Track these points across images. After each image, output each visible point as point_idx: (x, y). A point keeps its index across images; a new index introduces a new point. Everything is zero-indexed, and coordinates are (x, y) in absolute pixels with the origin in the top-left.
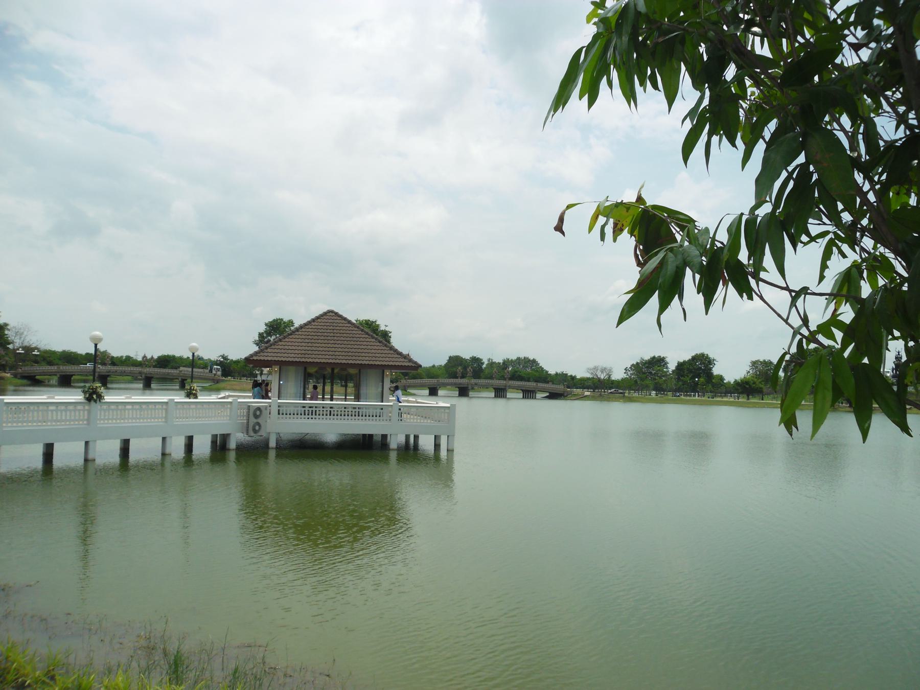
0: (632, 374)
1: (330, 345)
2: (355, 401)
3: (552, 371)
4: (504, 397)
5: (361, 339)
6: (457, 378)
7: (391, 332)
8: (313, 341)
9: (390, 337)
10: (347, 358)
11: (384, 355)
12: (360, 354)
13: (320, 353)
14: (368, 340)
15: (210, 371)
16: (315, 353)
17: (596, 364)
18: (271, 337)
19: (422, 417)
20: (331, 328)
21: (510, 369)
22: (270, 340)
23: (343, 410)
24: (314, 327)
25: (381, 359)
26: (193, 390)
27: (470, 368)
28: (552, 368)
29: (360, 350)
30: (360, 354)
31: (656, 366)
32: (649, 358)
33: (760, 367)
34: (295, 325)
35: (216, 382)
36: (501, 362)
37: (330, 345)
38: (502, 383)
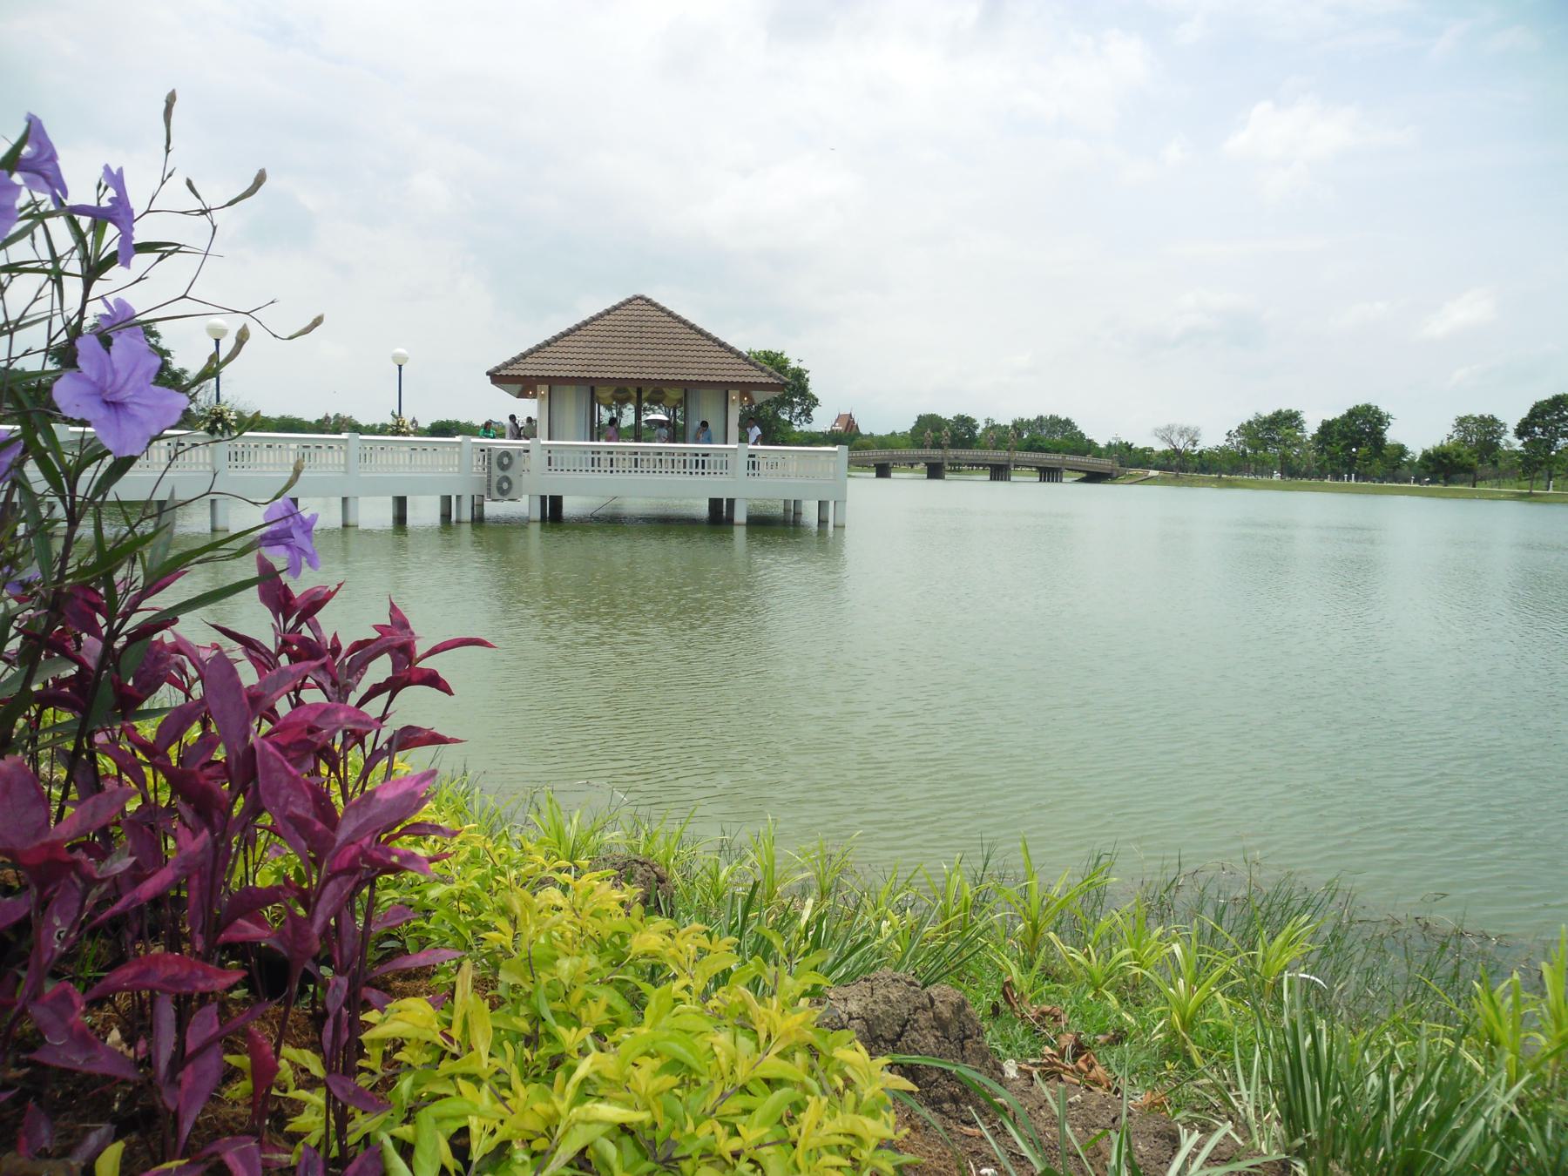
0: (1238, 442)
7: (808, 372)
9: (808, 380)
10: (661, 370)
14: (699, 342)
17: (1172, 422)
20: (638, 323)
21: (1025, 436)
26: (403, 426)
29: (684, 359)
31: (1284, 428)
33: (1473, 427)
37: (633, 351)
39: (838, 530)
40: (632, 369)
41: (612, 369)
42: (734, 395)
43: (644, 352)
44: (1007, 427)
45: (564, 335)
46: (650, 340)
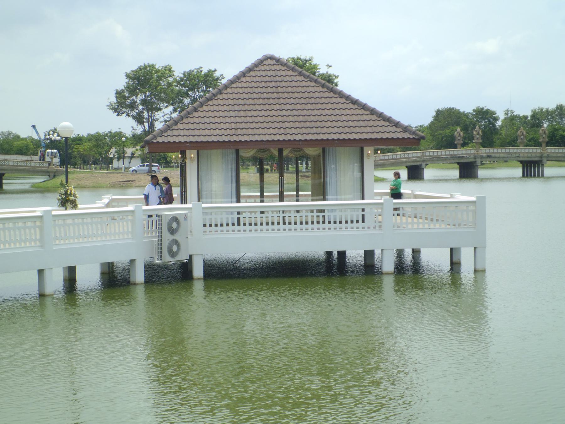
1: (273, 113)
2: (312, 200)
4: (539, 176)
5: (323, 100)
6: (455, 147)
7: (337, 77)
8: (246, 107)
10: (304, 130)
11: (362, 123)
12: (324, 124)
13: (259, 125)
14: (334, 100)
15: (40, 157)
16: (252, 126)
18: (137, 96)
19: (426, 219)
20: (273, 84)
22: (136, 102)
23: (258, 215)
24: (245, 85)
26: (70, 194)
27: (477, 128)
29: (323, 118)
34: (174, 73)
35: (52, 175)
38: (533, 152)
39: (479, 274)
40: (276, 131)
41: (258, 132)
43: (284, 113)
44: (526, 117)
46: (287, 101)
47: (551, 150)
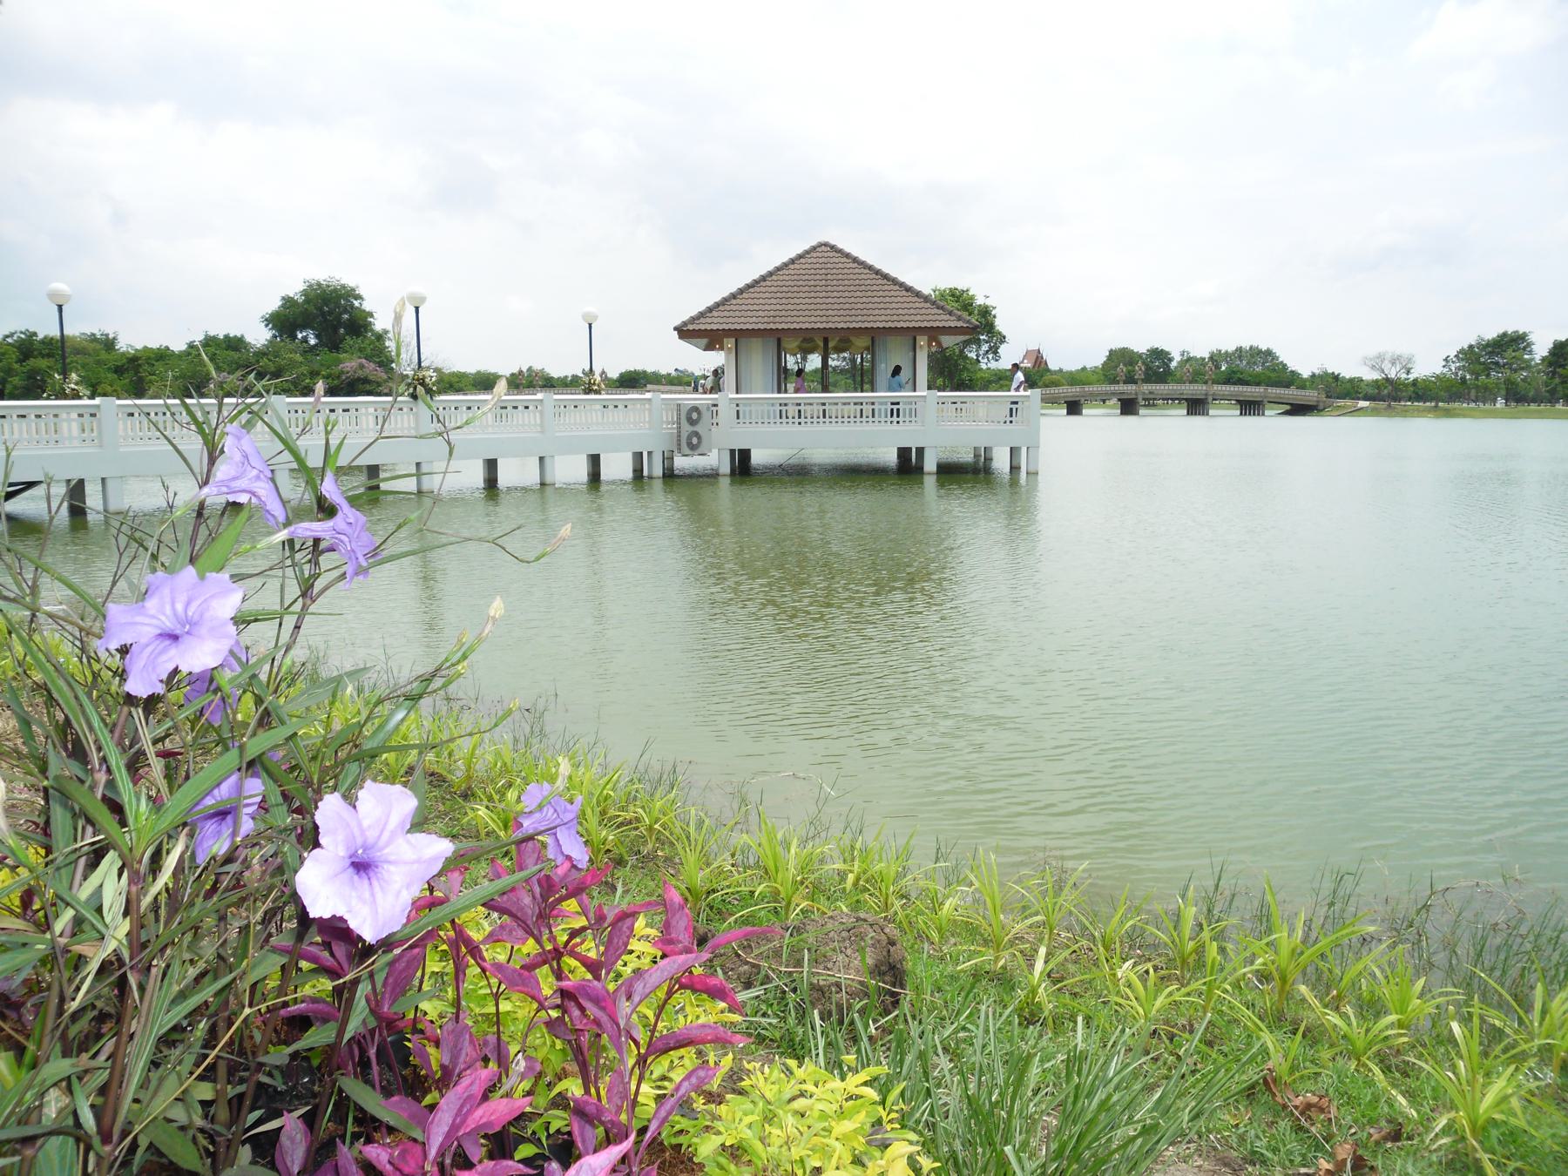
1: (818, 300)
3: (1306, 374)
5: (875, 288)
7: (994, 308)
8: (789, 295)
9: (995, 317)
10: (848, 318)
12: (870, 312)
13: (801, 313)
14: (886, 287)
21: (1223, 368)
25: (907, 317)
26: (594, 384)
27: (1140, 364)
28: (1304, 366)
29: (870, 306)
30: (870, 312)
32: (1495, 335)
36: (1207, 356)
37: (818, 300)
42: (922, 341)
43: (830, 300)
45: (749, 286)
47: (1218, 388)
